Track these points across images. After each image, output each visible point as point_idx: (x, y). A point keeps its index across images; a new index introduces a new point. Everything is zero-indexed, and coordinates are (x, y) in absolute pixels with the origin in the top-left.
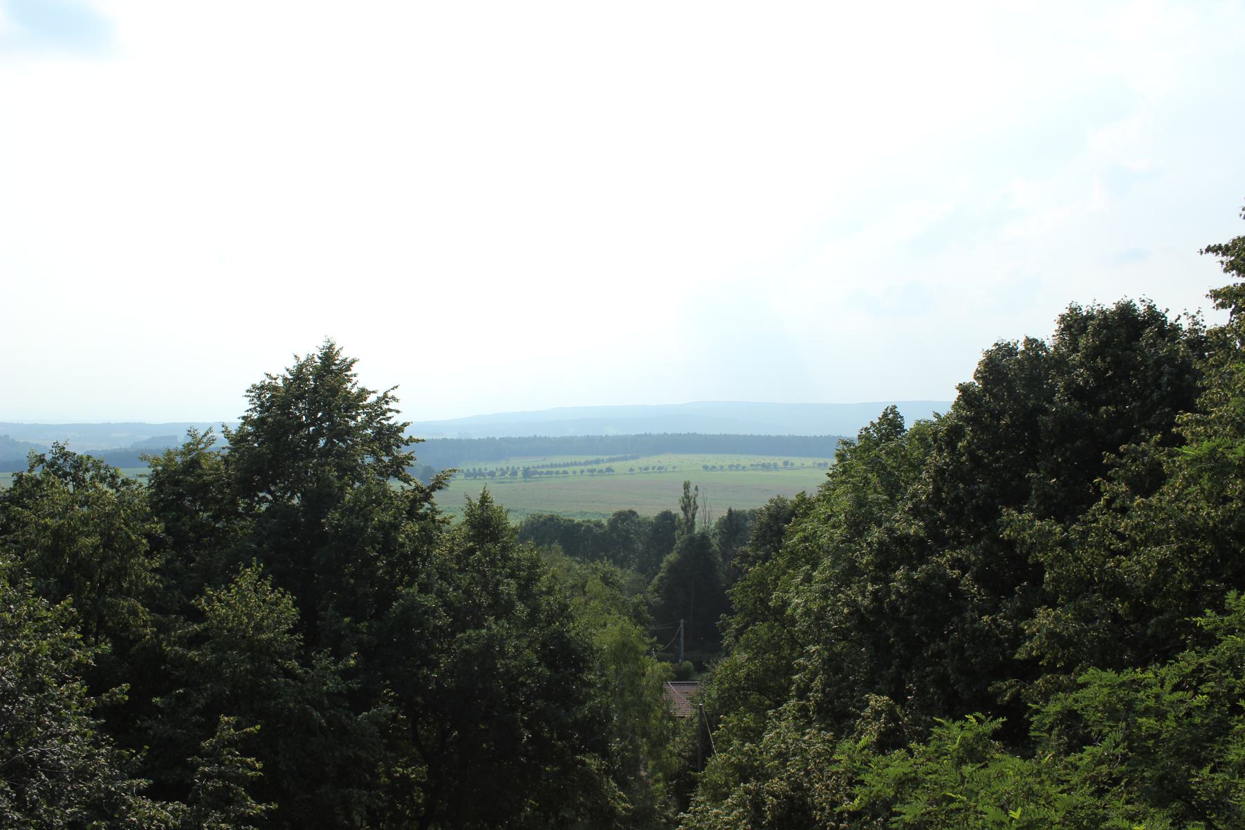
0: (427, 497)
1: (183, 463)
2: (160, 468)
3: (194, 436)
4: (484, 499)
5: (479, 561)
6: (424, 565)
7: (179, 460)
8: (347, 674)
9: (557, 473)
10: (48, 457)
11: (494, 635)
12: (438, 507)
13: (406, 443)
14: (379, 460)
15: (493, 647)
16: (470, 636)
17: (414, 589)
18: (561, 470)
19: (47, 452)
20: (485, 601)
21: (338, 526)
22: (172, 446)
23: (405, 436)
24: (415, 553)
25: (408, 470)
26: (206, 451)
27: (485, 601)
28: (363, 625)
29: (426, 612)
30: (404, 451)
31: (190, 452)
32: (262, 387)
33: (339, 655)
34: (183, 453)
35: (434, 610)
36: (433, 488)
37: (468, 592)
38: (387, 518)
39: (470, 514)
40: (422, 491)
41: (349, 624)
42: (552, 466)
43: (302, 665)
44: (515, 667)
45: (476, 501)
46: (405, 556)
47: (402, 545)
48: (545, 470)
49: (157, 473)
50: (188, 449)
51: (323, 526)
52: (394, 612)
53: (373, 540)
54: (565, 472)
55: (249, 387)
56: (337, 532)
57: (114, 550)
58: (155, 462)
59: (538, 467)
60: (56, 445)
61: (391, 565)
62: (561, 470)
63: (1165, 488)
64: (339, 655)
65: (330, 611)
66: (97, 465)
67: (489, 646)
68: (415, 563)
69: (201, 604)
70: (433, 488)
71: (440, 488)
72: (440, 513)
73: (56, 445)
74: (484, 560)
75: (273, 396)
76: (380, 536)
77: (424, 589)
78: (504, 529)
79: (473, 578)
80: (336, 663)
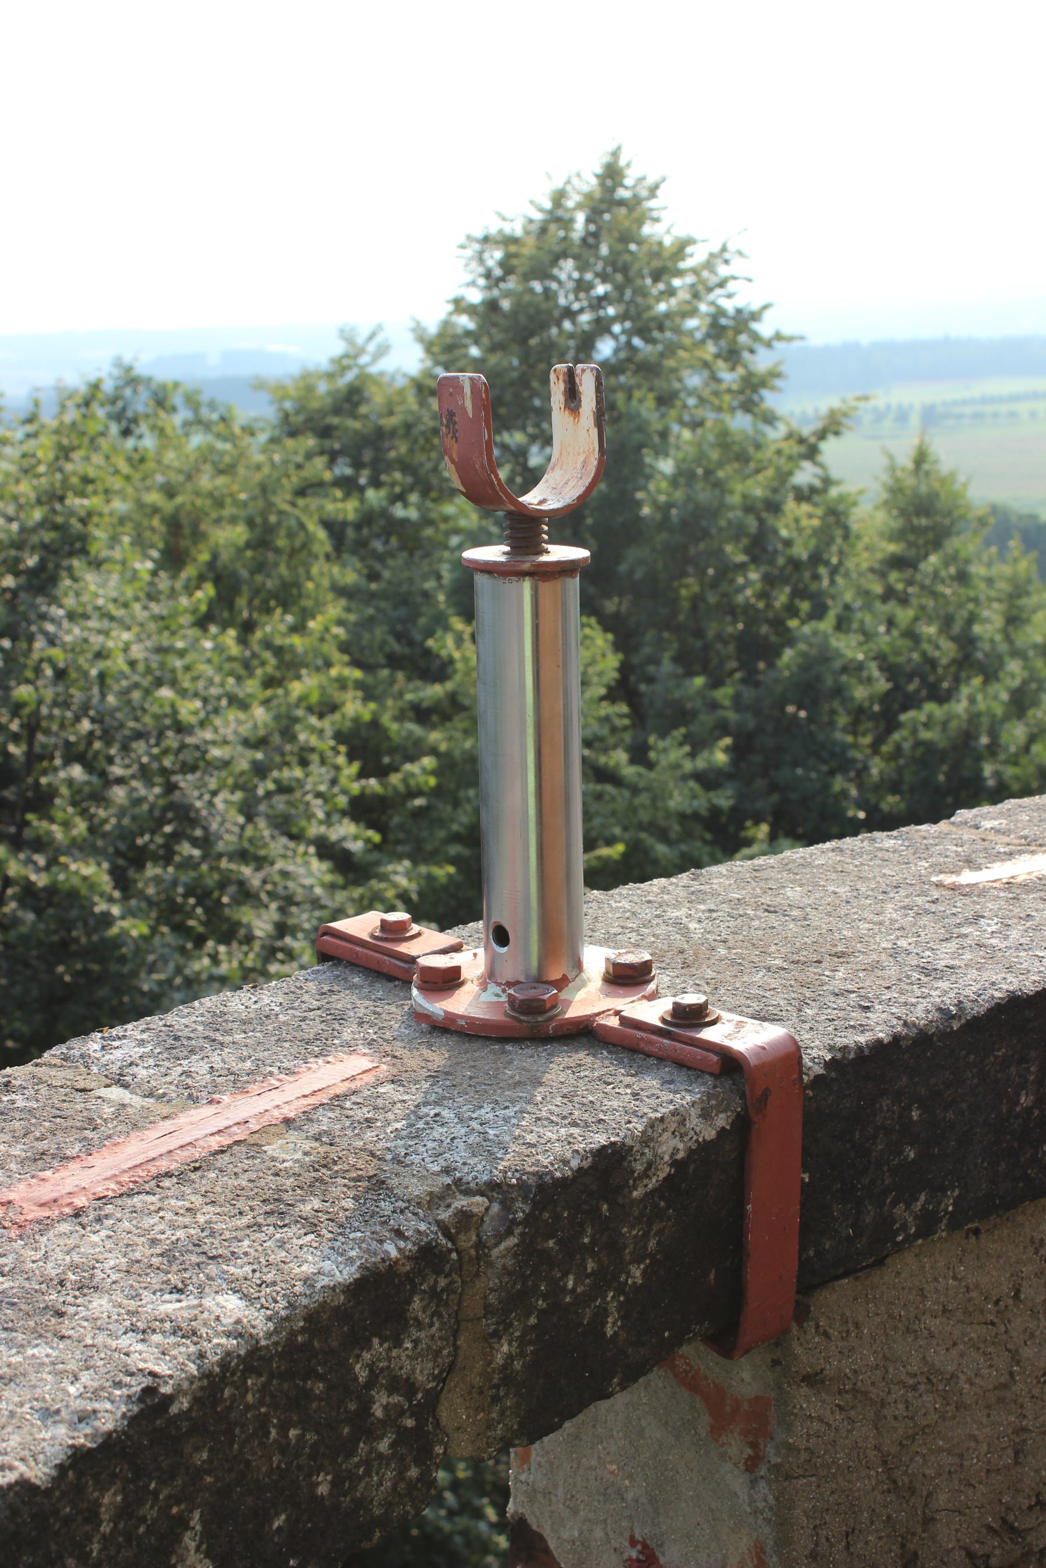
0: (811, 453)
1: (329, 393)
2: (288, 405)
3: (350, 341)
4: (921, 458)
5: (936, 574)
6: (832, 582)
7: (322, 387)
8: (708, 780)
9: (995, 415)
10: (108, 387)
11: (979, 715)
12: (835, 474)
13: (768, 344)
14: (715, 378)
15: (977, 738)
16: (930, 716)
17: (826, 625)
18: (1004, 409)
19: (103, 374)
20: (947, 650)
21: (669, 505)
22: (311, 367)
23: (764, 328)
24: (816, 558)
25: (770, 400)
26: (373, 370)
27: (947, 650)
28: (724, 694)
29: (844, 670)
30: (762, 361)
31: (344, 369)
32: (486, 240)
33: (697, 745)
34: (330, 376)
35: (860, 667)
36: (822, 435)
37: (911, 635)
38: (758, 491)
39: (896, 490)
40: (801, 441)
41: (700, 692)
42: (984, 400)
43: (633, 761)
44: (1017, 778)
45: (905, 461)
46: (795, 564)
47: (788, 543)
48: (968, 410)
49: (287, 416)
50: (341, 364)
51: (639, 504)
52: (788, 667)
53: (738, 532)
54: (1012, 415)
55: (462, 240)
56: (666, 517)
57: (278, 551)
58: (279, 392)
59: (955, 403)
60: (118, 363)
61: (770, 581)
62: (1004, 409)
63: (196, 1003)
64: (697, 745)
65: (667, 666)
66: (192, 401)
67: (968, 736)
68: (816, 577)
69: (444, 647)
70: (822, 435)
71: (837, 433)
72: (837, 483)
73: (118, 363)
74: (943, 574)
75: (508, 256)
76: (752, 524)
77: (842, 625)
78: (962, 517)
79: (922, 608)
80: (692, 755)
